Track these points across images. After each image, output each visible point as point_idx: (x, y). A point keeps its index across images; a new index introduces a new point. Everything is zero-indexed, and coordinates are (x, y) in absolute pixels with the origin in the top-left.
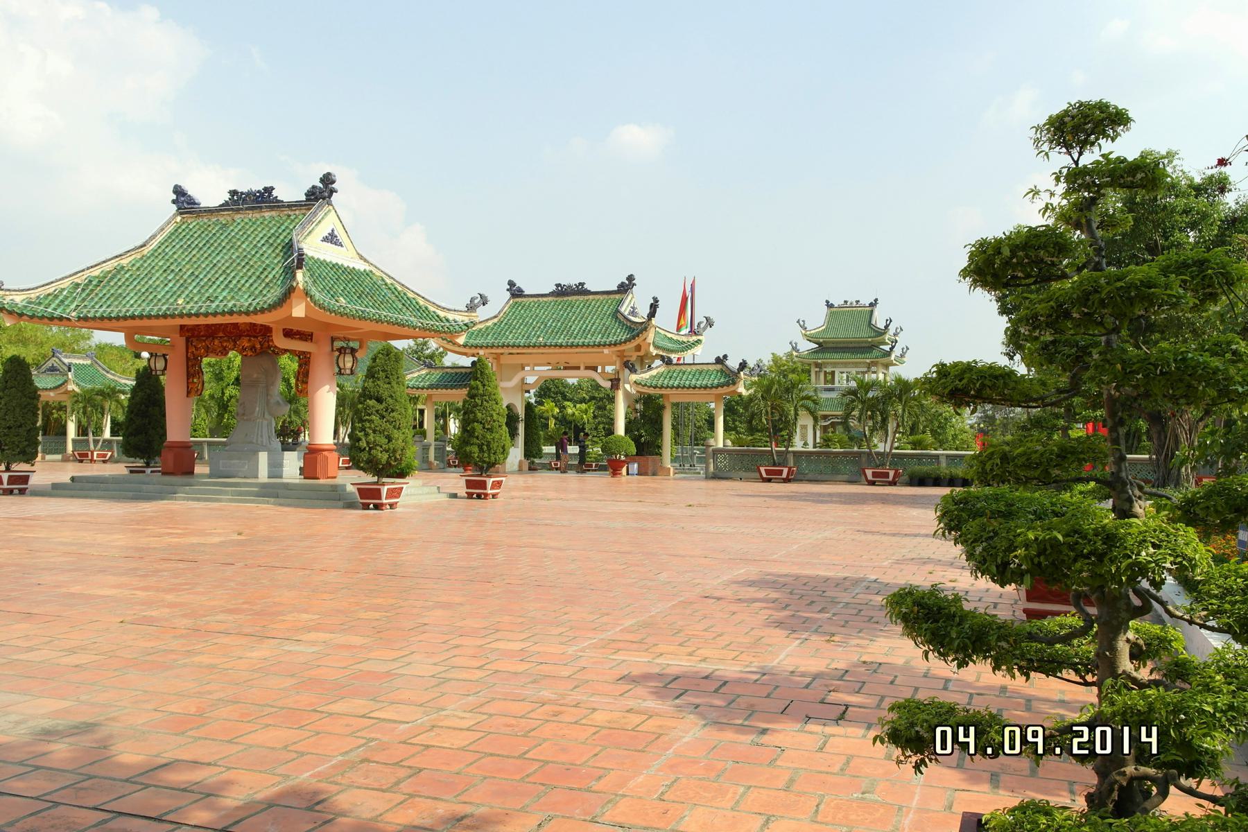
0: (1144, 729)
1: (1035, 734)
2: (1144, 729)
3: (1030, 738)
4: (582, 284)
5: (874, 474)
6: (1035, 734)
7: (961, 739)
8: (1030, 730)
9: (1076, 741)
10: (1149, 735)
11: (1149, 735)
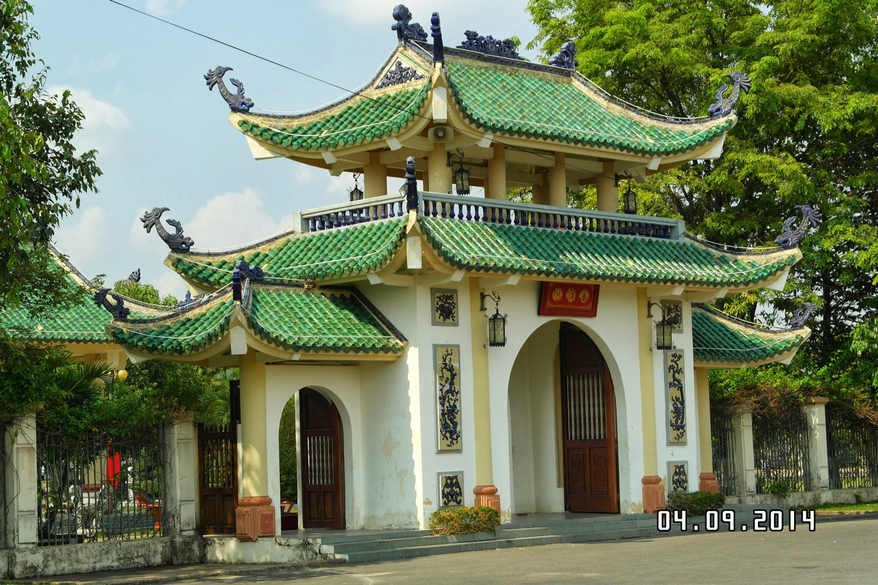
0: (805, 513)
1: (728, 516)
2: (805, 513)
3: (725, 519)
4: (74, 149)
5: (728, 248)
6: (728, 516)
7: (676, 519)
8: (725, 513)
9: (757, 521)
10: (680, 517)
11: (680, 517)
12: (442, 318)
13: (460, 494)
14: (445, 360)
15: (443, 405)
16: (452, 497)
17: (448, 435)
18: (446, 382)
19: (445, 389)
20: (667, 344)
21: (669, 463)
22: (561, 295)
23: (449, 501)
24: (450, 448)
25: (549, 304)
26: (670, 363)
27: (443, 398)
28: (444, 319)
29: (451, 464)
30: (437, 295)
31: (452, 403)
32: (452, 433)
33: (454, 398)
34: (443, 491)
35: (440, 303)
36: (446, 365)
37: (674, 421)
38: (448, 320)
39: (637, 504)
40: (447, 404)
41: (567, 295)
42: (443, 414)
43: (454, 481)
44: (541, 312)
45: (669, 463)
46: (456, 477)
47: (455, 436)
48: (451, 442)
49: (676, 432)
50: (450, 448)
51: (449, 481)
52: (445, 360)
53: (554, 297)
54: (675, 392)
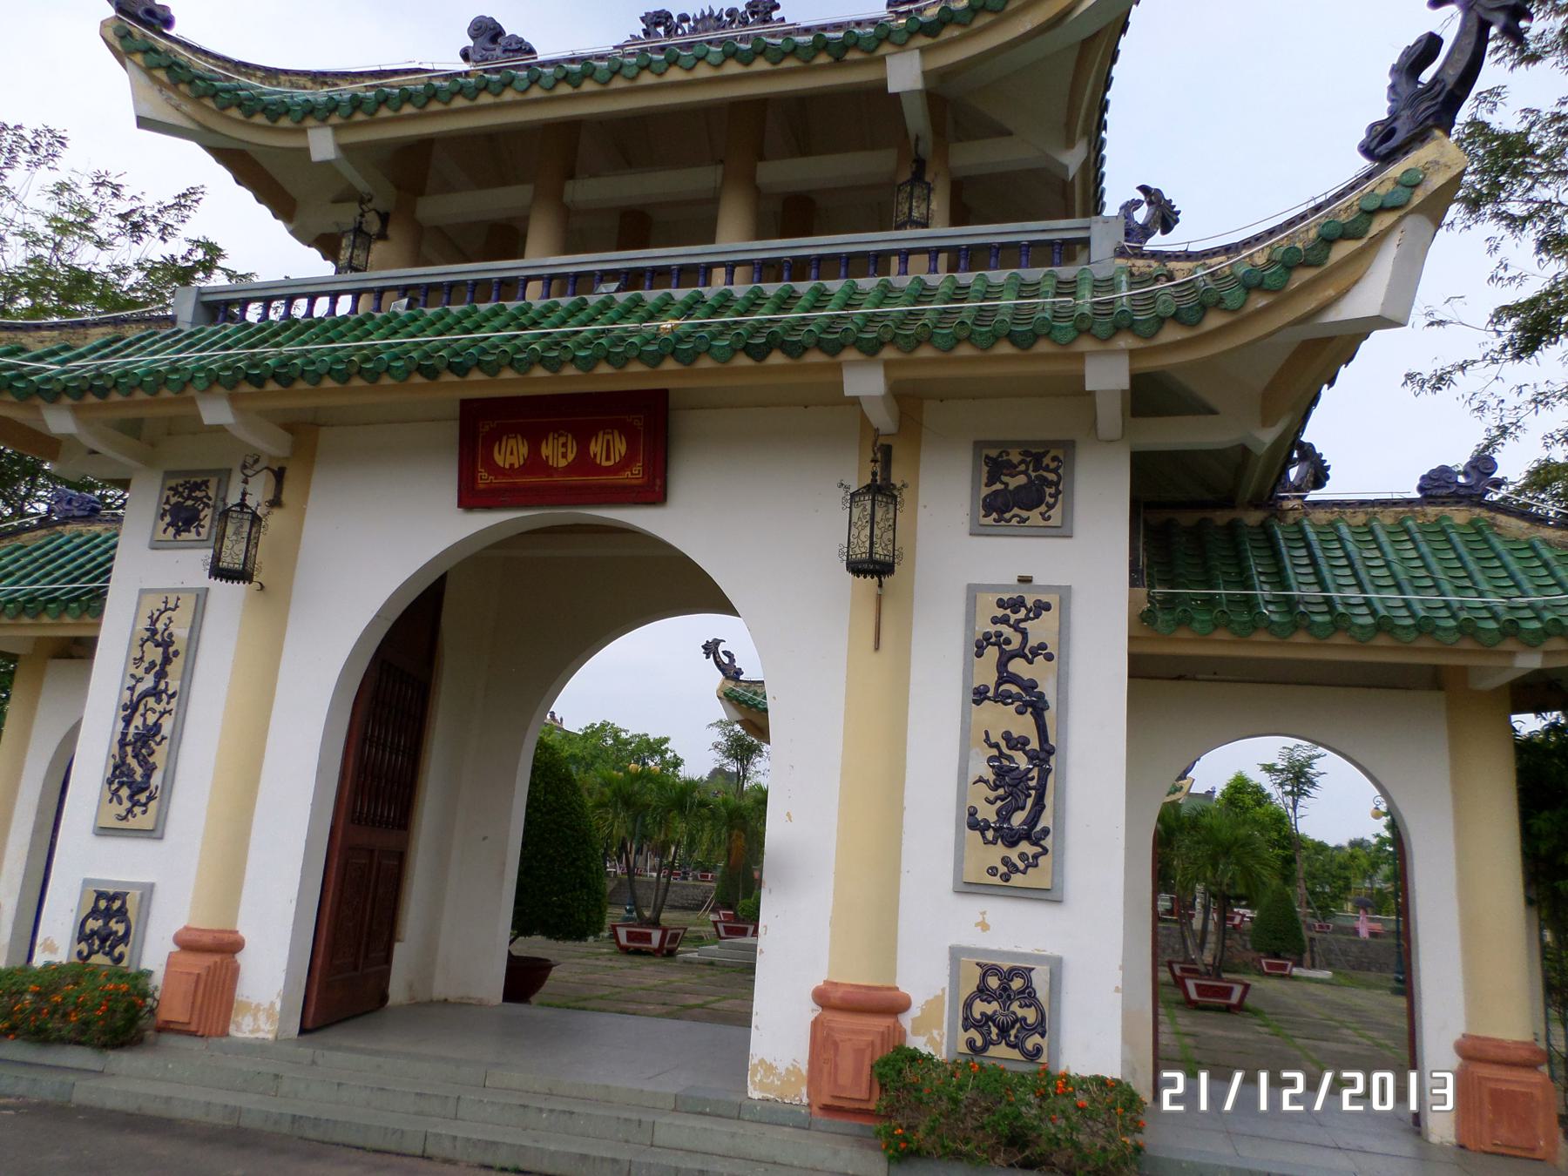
12: (171, 530)
13: (1040, 1028)
14: (154, 622)
15: (128, 721)
16: (103, 941)
17: (125, 792)
18: (147, 671)
19: (141, 688)
20: (880, 553)
21: (956, 954)
22: (524, 450)
23: (988, 1043)
24: (123, 824)
25: (484, 478)
26: (985, 626)
27: (131, 709)
28: (178, 532)
29: (122, 863)
30: (173, 483)
31: (151, 719)
32: (137, 789)
33: (159, 708)
34: (968, 1005)
35: (173, 500)
36: (154, 632)
37: (988, 813)
38: (184, 535)
39: (782, 1069)
40: (137, 721)
41: (546, 451)
42: (123, 743)
43: (117, 905)
44: (470, 498)
45: (956, 954)
46: (1025, 973)
47: (143, 797)
48: (130, 811)
49: (1000, 850)
50: (123, 824)
51: (993, 982)
52: (154, 622)
53: (499, 459)
54: (1006, 720)
